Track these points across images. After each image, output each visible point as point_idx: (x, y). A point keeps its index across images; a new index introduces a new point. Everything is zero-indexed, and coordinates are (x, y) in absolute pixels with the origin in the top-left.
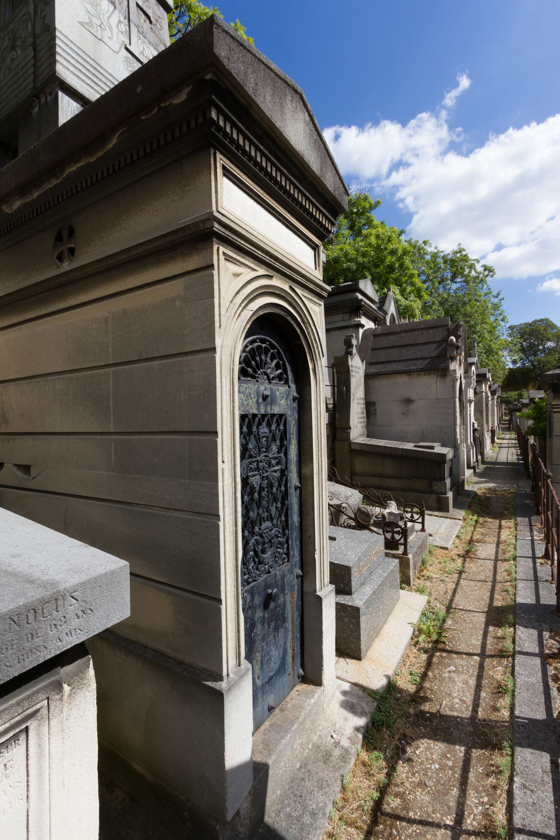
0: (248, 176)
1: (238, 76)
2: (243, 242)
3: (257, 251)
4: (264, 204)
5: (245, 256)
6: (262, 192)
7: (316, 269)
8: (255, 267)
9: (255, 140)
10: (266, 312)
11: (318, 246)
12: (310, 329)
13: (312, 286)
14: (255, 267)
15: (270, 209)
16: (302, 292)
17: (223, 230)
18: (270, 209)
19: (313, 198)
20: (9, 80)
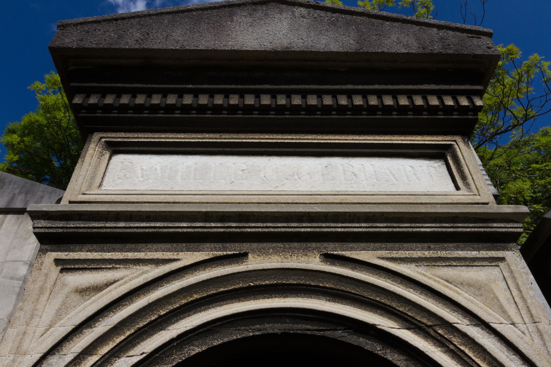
0: (172, 132)
1: (423, 29)
2: (122, 224)
3: (170, 225)
4: (277, 150)
5: (140, 246)
6: (218, 136)
7: (457, 188)
8: (168, 255)
9: (213, 86)
10: (226, 340)
11: (449, 147)
12: (456, 341)
13: (427, 228)
14: (168, 255)
15: (345, 150)
16: (384, 253)
17: (61, 224)
18: (345, 150)
19: (373, 84)
20: (519, 330)
